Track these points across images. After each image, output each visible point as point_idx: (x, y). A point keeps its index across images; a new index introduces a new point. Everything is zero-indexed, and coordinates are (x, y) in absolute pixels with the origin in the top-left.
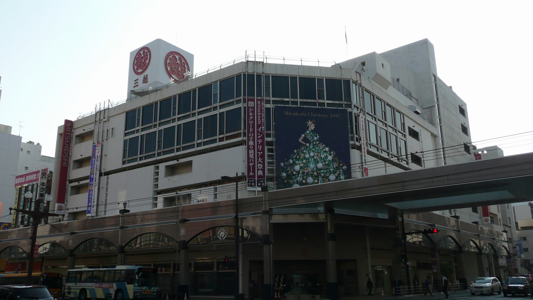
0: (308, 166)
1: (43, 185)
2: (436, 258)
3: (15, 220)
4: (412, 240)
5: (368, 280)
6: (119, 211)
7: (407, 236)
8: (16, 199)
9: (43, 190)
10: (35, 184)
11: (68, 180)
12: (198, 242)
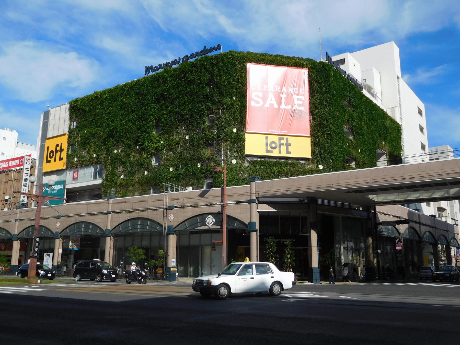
0: (245, 159)
1: (27, 170)
4: (382, 229)
5: (62, 152)
7: (378, 226)
9: (26, 175)
11: (148, 270)
12: (186, 227)
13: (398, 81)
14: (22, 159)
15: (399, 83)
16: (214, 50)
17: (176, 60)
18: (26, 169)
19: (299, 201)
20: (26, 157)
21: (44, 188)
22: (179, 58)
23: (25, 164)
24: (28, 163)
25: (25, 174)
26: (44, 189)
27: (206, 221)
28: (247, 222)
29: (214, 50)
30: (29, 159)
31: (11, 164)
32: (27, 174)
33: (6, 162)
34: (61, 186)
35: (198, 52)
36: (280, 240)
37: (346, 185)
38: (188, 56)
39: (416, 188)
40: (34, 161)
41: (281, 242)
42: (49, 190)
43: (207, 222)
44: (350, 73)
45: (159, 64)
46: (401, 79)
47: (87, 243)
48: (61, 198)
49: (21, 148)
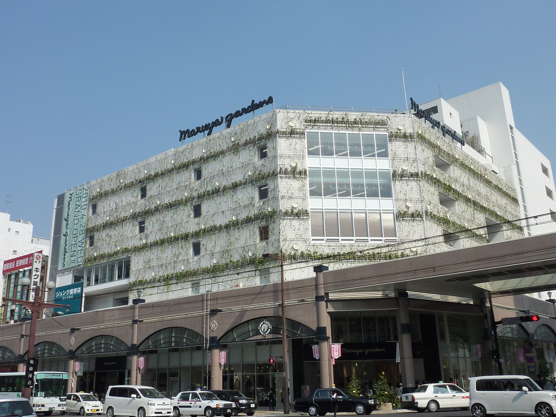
1: (37, 271)
2: (532, 353)
3: (3, 315)
6: (132, 301)
7: (497, 325)
8: (4, 289)
10: (27, 270)
13: (512, 132)
14: (31, 257)
15: (513, 134)
16: (264, 104)
17: (217, 120)
18: (36, 270)
19: (384, 295)
20: (36, 254)
21: (57, 293)
22: (222, 117)
23: (35, 263)
24: (38, 262)
25: (34, 276)
26: (58, 294)
27: (260, 328)
28: (314, 327)
29: (264, 105)
30: (39, 256)
31: (19, 264)
32: (37, 276)
33: (13, 262)
34: (79, 290)
35: (245, 108)
36: (364, 350)
37: (434, 268)
38: (232, 114)
39: (542, 270)
40: (45, 260)
41: (366, 354)
42: (64, 295)
43: (261, 330)
44: (446, 124)
45: (197, 127)
46: (516, 129)
47: (111, 363)
48: (62, 305)
49: (37, 243)
